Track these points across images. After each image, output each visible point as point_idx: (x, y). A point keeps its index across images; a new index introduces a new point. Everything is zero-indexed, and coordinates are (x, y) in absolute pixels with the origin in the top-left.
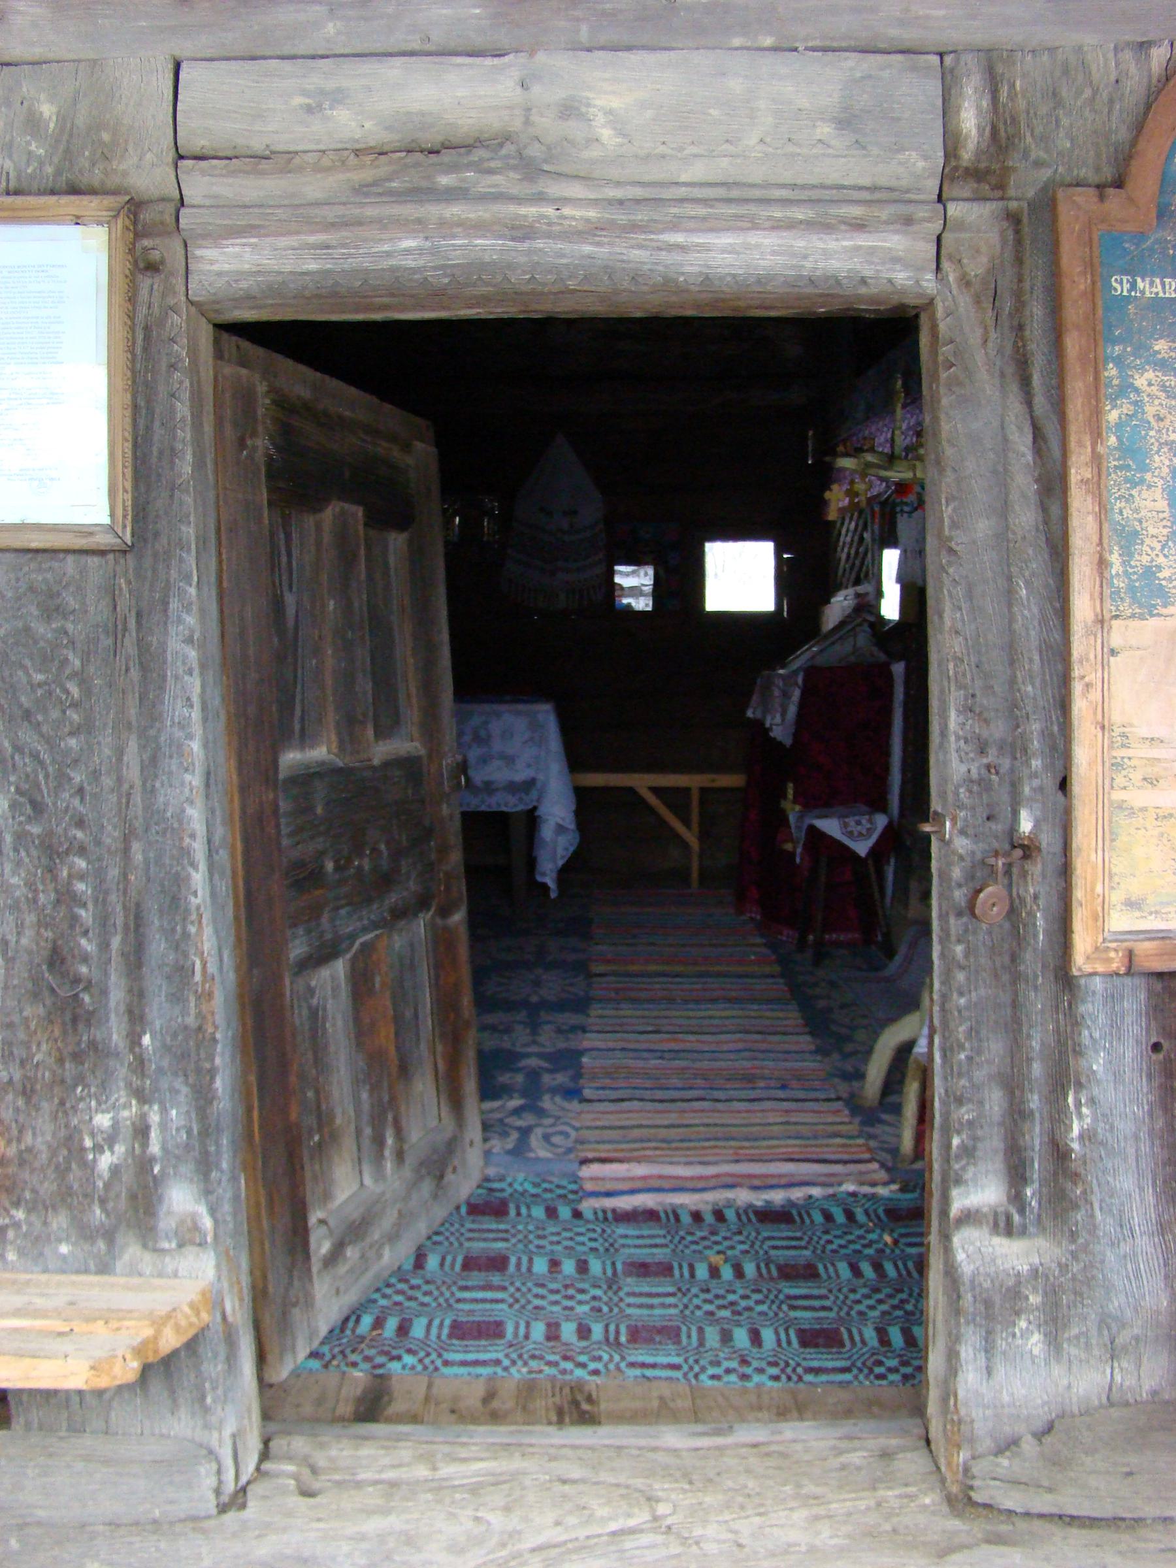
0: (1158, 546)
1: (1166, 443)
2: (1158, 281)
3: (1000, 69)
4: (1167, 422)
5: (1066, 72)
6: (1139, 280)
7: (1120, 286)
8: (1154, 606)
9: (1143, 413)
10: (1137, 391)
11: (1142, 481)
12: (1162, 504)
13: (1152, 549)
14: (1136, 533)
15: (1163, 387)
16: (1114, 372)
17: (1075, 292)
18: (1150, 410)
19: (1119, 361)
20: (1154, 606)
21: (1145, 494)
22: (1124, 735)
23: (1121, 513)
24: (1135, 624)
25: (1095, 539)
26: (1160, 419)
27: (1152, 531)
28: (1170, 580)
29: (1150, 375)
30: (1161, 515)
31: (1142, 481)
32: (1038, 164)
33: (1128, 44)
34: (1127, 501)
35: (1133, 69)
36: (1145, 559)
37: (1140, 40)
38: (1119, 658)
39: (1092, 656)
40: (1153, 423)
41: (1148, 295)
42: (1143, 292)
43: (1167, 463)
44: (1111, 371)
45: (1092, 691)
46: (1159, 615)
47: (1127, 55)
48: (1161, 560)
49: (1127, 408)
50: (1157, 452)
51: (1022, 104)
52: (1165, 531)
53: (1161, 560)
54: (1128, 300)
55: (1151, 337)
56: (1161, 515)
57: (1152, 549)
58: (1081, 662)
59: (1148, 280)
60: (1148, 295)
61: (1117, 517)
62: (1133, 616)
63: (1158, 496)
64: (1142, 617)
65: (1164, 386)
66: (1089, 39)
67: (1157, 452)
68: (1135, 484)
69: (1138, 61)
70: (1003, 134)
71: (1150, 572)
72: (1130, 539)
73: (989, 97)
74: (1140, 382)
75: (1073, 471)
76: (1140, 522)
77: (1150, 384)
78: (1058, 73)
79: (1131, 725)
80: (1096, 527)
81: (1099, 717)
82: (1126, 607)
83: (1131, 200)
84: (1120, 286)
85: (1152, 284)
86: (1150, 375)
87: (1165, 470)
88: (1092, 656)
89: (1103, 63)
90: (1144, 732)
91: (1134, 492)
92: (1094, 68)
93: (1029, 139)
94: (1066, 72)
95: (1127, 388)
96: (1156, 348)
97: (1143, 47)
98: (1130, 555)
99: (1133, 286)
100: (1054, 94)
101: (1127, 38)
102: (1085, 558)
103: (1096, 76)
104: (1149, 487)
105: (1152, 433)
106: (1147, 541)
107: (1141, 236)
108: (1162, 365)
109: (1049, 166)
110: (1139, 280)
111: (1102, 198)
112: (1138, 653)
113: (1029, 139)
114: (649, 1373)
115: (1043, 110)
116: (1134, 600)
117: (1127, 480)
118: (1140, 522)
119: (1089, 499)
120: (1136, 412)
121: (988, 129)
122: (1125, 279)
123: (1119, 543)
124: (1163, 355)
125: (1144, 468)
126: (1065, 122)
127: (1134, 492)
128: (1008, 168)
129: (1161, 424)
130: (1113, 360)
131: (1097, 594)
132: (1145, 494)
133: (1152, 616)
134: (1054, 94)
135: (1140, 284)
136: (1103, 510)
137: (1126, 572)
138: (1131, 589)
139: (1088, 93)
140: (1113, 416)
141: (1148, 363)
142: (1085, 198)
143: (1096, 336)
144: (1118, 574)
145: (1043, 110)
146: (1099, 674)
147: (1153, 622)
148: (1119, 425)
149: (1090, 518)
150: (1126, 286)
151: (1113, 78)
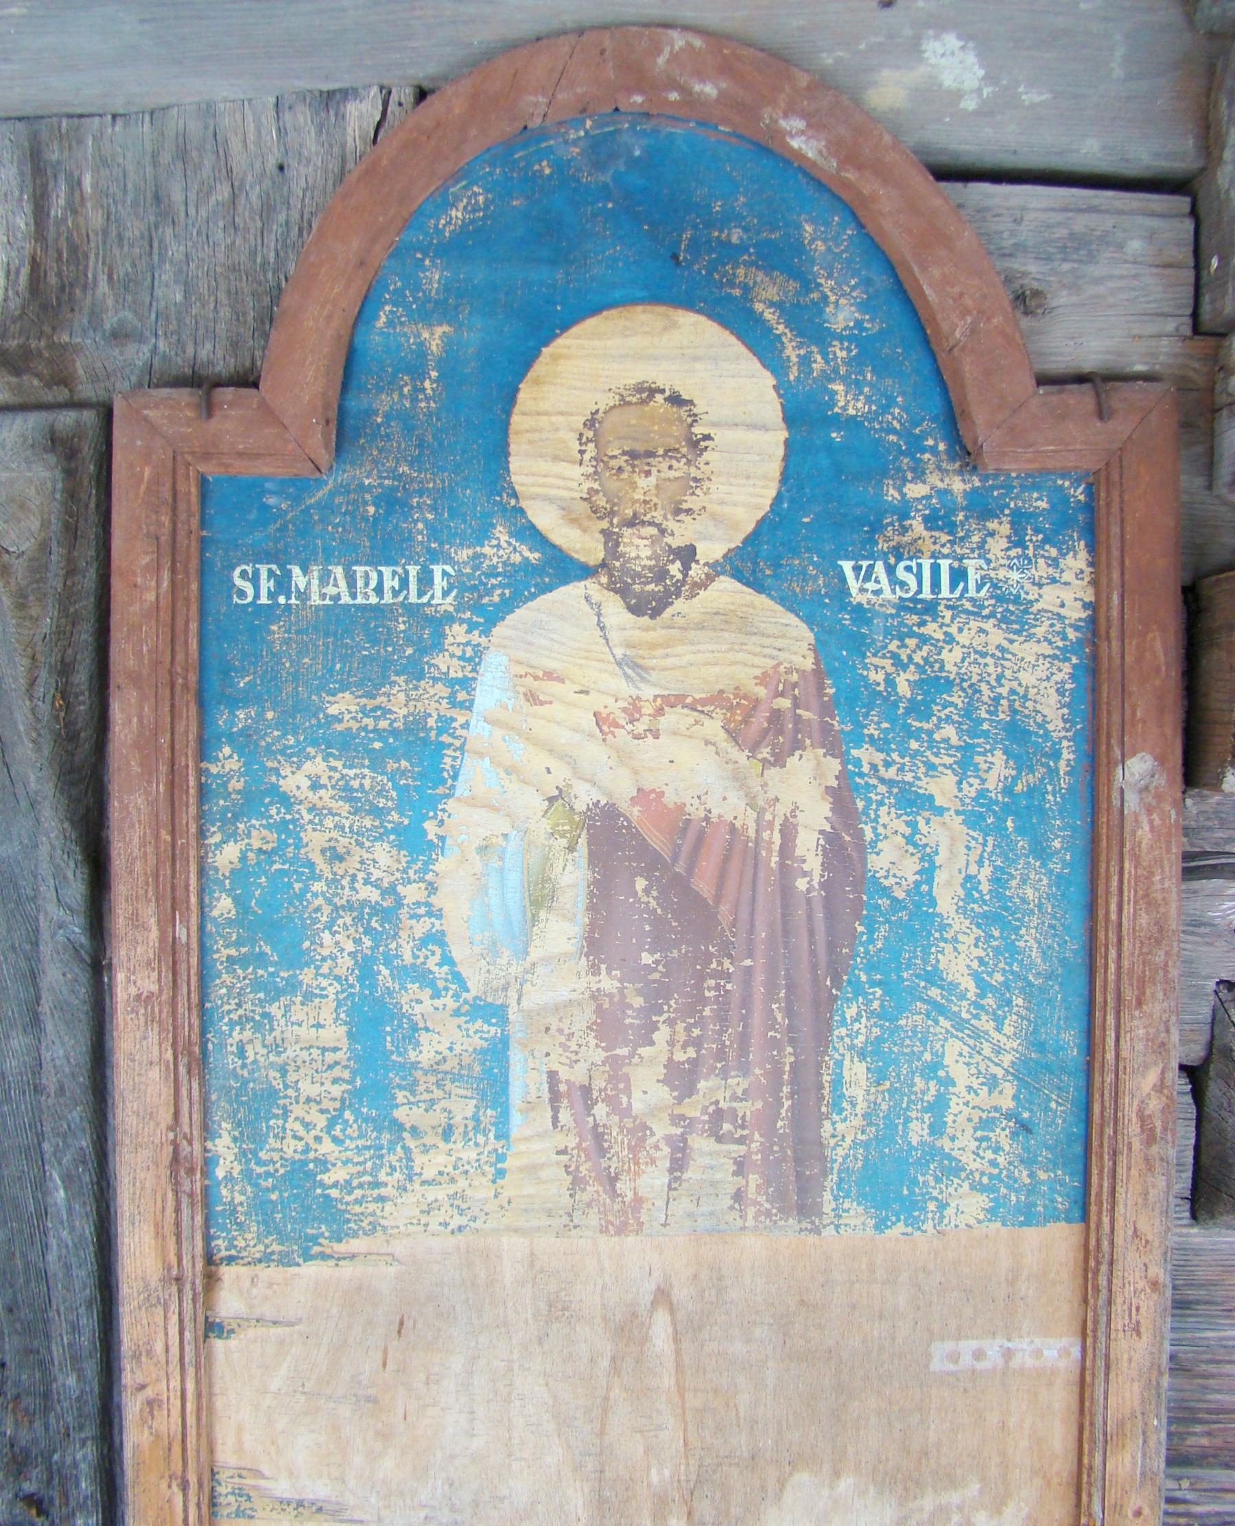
0: (321, 1121)
1: (349, 907)
2: (339, 571)
3: (53, 154)
4: (353, 863)
5: (182, 154)
6: (296, 571)
7: (251, 585)
8: (314, 1239)
9: (299, 845)
10: (286, 800)
11: (293, 986)
12: (335, 1034)
13: (307, 1126)
14: (273, 1094)
15: (347, 792)
16: (234, 764)
17: (136, 608)
18: (315, 840)
19: (245, 742)
20: (314, 1239)
21: (298, 1013)
22: (239, 1492)
23: (241, 1053)
24: (268, 1273)
25: (166, 1117)
26: (335, 856)
27: (307, 1089)
28: (348, 1186)
29: (317, 766)
30: (330, 1057)
31: (293, 986)
32: (119, 336)
33: (302, 96)
34: (258, 1027)
35: (311, 143)
36: (291, 1147)
37: (326, 87)
38: (233, 1343)
39: (159, 1347)
40: (321, 864)
41: (315, 600)
42: (304, 596)
43: (350, 946)
44: (227, 762)
45: (160, 1415)
46: (324, 1256)
47: (302, 117)
48: (327, 1147)
49: (260, 837)
50: (329, 926)
51: (94, 218)
52: (337, 1091)
53: (327, 1147)
54: (269, 613)
55: (321, 688)
56: (330, 1057)
57: (307, 1126)
58: (137, 1356)
59: (315, 570)
60: (315, 600)
61: (232, 1062)
62: (266, 1259)
63: (327, 1015)
64: (286, 1260)
65: (348, 789)
66: (223, 89)
67: (329, 926)
68: (275, 993)
69: (320, 128)
70: (53, 280)
71: (302, 1173)
72: (259, 1107)
73: (28, 208)
74: (294, 781)
75: (120, 977)
76: (283, 1071)
77: (315, 786)
78: (166, 157)
79: (257, 1473)
80: (167, 1092)
81: (177, 1466)
82: (249, 1240)
83: (268, 414)
84: (251, 585)
85: (325, 579)
86: (317, 766)
87: (346, 962)
88: (159, 1347)
89: (252, 139)
90: (282, 1487)
91: (275, 1009)
92: (235, 146)
93: (103, 286)
94: (182, 154)
95: (261, 795)
96: (333, 710)
97: (331, 100)
98: (259, 1139)
99: (283, 584)
100: (157, 199)
101: (303, 84)
102: (144, 1153)
103: (239, 160)
104: (308, 997)
105: (318, 886)
106: (297, 1110)
107: (297, 487)
108: (345, 745)
109: (141, 339)
110: (296, 571)
111: (209, 408)
112: (275, 1331)
113: (103, 286)
114: (177, 1450)
115: (134, 229)
116: (269, 1227)
117: (257, 985)
118: (283, 1071)
119: (153, 1036)
120: (282, 845)
121: (25, 271)
122: (263, 570)
123: (232, 1116)
124: (348, 723)
125: (297, 958)
126: (176, 251)
127: (275, 1009)
128: (64, 347)
129: (339, 868)
130: (231, 739)
131: (169, 1228)
132: (298, 1013)
133: (308, 1257)
134: (157, 199)
135: (299, 579)
136: (194, 1057)
137: (248, 1174)
138: (261, 1206)
139: (223, 192)
140: (226, 856)
141: (315, 743)
142: (171, 411)
143: (197, 691)
144: (229, 1177)
145: (134, 229)
146: (175, 1383)
147: (311, 1271)
148: (241, 873)
149: (155, 1073)
150: (266, 585)
151: (272, 163)
